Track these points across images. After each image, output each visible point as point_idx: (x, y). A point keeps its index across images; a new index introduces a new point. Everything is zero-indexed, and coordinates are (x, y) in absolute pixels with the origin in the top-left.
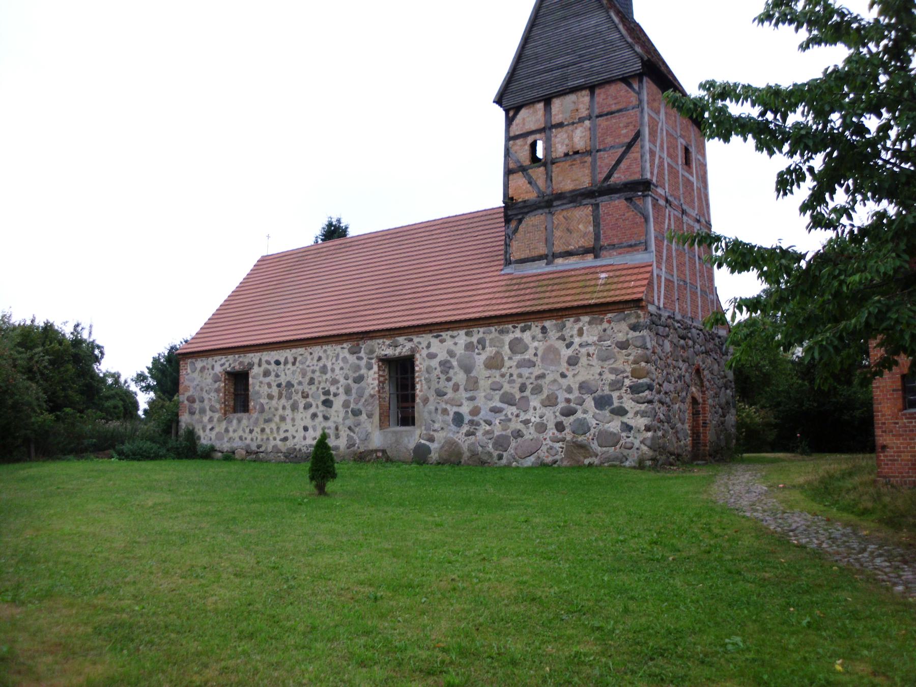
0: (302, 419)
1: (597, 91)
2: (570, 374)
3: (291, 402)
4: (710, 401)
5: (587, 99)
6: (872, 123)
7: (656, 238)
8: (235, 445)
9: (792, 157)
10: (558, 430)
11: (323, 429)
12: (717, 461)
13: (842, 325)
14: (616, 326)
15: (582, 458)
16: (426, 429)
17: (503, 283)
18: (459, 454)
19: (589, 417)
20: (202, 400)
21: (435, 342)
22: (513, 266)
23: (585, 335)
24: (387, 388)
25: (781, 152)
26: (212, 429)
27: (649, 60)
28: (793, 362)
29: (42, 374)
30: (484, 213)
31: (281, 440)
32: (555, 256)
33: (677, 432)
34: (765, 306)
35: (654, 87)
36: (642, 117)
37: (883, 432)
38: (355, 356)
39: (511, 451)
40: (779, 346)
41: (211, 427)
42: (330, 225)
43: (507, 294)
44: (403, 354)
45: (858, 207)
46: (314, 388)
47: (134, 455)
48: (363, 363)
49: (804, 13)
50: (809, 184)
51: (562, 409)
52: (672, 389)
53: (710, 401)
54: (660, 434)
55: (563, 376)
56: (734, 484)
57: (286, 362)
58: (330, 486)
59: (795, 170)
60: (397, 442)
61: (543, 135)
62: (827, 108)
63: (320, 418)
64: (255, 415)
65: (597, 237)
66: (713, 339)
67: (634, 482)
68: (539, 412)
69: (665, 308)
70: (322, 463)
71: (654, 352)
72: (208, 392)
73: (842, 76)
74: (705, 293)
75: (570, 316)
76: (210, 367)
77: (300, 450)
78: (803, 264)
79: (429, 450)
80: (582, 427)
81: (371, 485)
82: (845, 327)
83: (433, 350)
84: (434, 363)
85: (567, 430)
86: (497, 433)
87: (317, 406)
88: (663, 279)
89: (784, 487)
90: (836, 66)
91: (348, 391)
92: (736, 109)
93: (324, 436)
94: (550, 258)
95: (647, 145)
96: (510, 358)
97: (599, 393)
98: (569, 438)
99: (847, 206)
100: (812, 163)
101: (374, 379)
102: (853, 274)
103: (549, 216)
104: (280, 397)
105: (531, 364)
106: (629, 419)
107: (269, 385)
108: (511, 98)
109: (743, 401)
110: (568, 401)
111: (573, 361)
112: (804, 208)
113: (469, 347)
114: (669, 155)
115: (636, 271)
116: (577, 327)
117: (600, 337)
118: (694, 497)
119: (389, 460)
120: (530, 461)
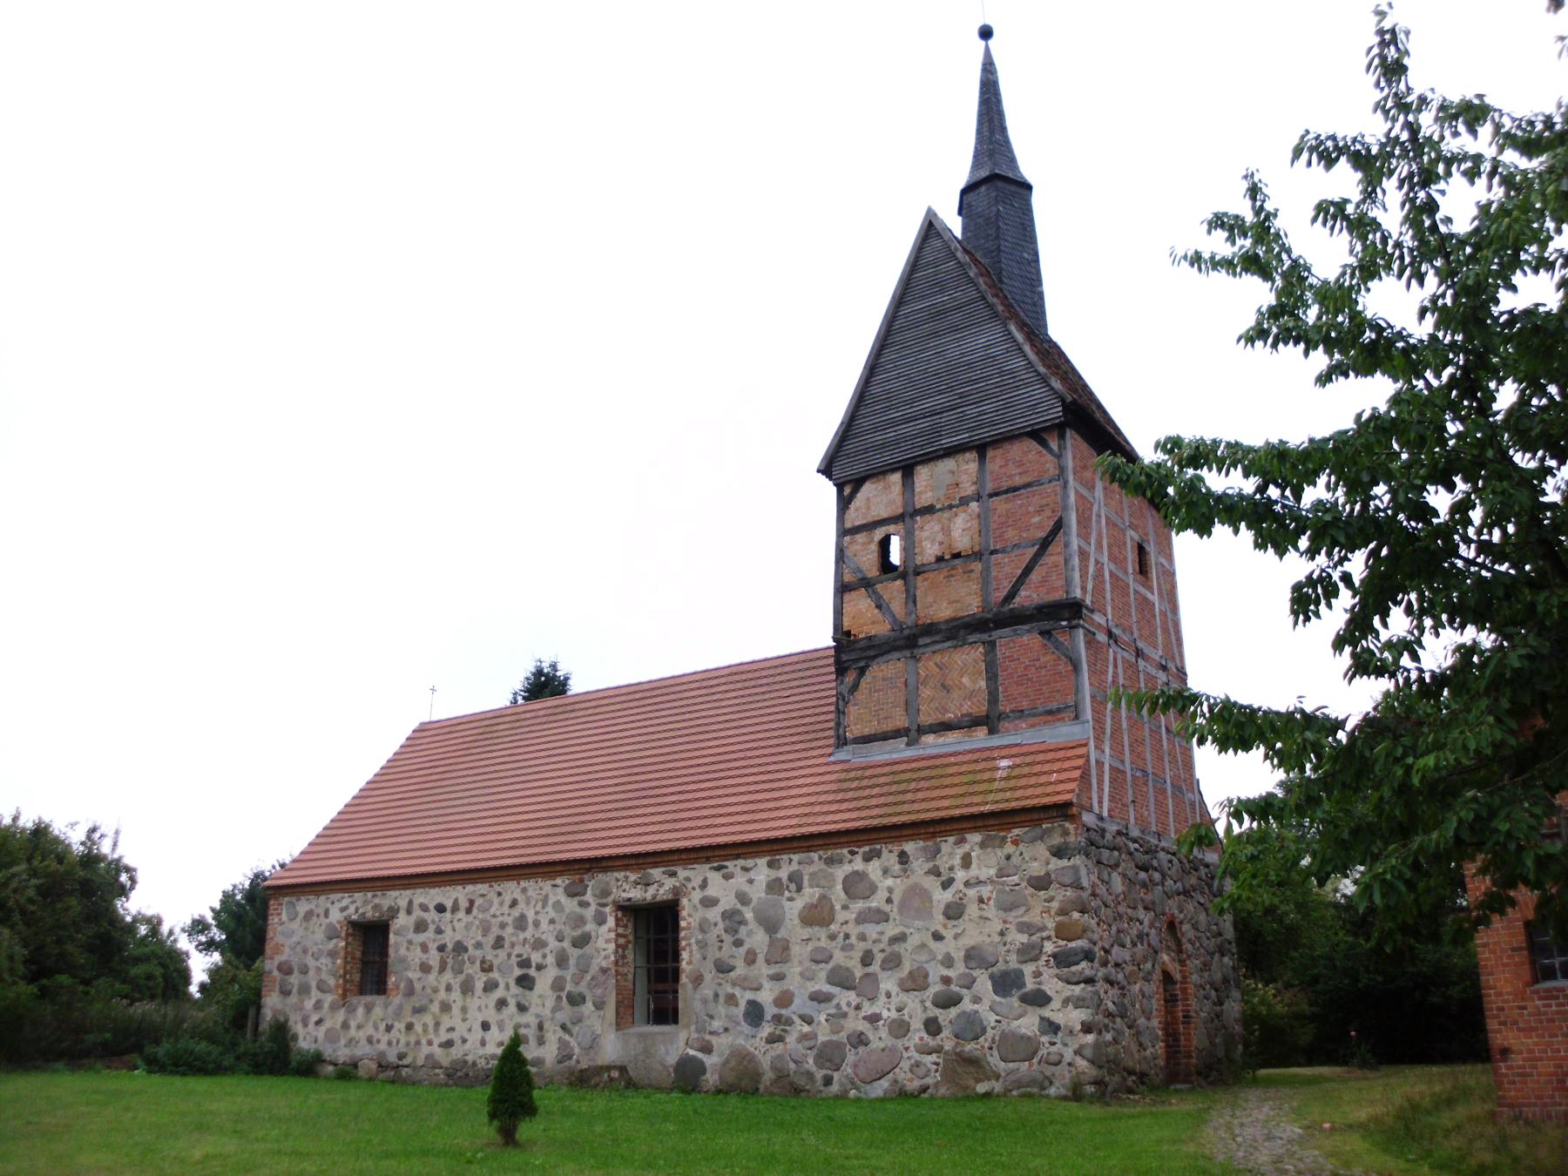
0: (480, 1009)
1: (990, 453)
2: (948, 934)
3: (461, 978)
4: (1195, 977)
5: (973, 467)
6: (1440, 500)
7: (1093, 697)
8: (358, 1052)
9: (1313, 558)
10: (928, 1032)
11: (517, 1027)
12: (1211, 1083)
13: (1416, 842)
14: (1027, 850)
15: (971, 1082)
16: (698, 1031)
17: (834, 777)
18: (756, 1075)
19: (983, 1009)
20: (304, 971)
21: (715, 878)
22: (850, 747)
23: (974, 866)
24: (630, 957)
25: (1297, 549)
26: (319, 1022)
27: (1074, 402)
28: (1336, 905)
29: (23, 912)
30: (802, 657)
31: (440, 1046)
32: (922, 730)
33: (1138, 1033)
34: (1281, 809)
35: (1084, 447)
36: (1065, 497)
37: (1501, 1023)
38: (577, 899)
39: (847, 1069)
40: (1308, 876)
41: (318, 1019)
42: (539, 673)
43: (840, 796)
44: (659, 898)
45: (1427, 638)
46: (502, 954)
47: (176, 1065)
48: (589, 913)
49: (1317, 327)
50: (1345, 599)
51: (936, 995)
52: (1128, 958)
53: (1195, 977)
54: (1108, 1037)
55: (938, 937)
56: (1242, 1125)
57: (455, 909)
58: (526, 1130)
59: (1320, 579)
60: (647, 1052)
61: (900, 526)
62: (1366, 478)
63: (512, 1008)
64: (397, 1000)
65: (993, 698)
66: (1196, 870)
67: (1065, 1124)
68: (895, 1001)
69: (1110, 816)
70: (511, 1089)
71: (1094, 895)
72: (316, 957)
73: (1387, 425)
74: (1181, 791)
75: (948, 833)
76: (321, 911)
77: (474, 1064)
78: (1342, 736)
79: (701, 1068)
80: (971, 1028)
81: (599, 1129)
82: (1421, 848)
83: (711, 892)
84: (714, 914)
85: (946, 1033)
86: (822, 1038)
87: (507, 987)
88: (1107, 767)
89: (1332, 1129)
90: (1374, 409)
91: (562, 961)
92: (1216, 481)
93: (517, 1041)
94: (913, 733)
95: (1075, 542)
96: (845, 907)
97: (1001, 966)
98: (948, 1046)
99: (1409, 637)
100: (1347, 566)
101: (608, 941)
102: (1427, 753)
103: (911, 662)
104: (442, 969)
105: (881, 917)
106: (1054, 1012)
107: (424, 948)
108: (846, 465)
109: (1254, 976)
110: (946, 980)
111: (954, 912)
112: (1338, 644)
113: (774, 887)
114: (1112, 558)
115: (1061, 754)
116: (960, 851)
117: (1000, 870)
118: (1173, 1148)
119: (631, 1084)
120: (880, 1088)
